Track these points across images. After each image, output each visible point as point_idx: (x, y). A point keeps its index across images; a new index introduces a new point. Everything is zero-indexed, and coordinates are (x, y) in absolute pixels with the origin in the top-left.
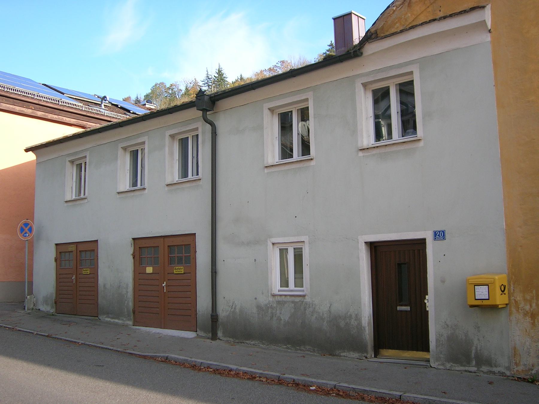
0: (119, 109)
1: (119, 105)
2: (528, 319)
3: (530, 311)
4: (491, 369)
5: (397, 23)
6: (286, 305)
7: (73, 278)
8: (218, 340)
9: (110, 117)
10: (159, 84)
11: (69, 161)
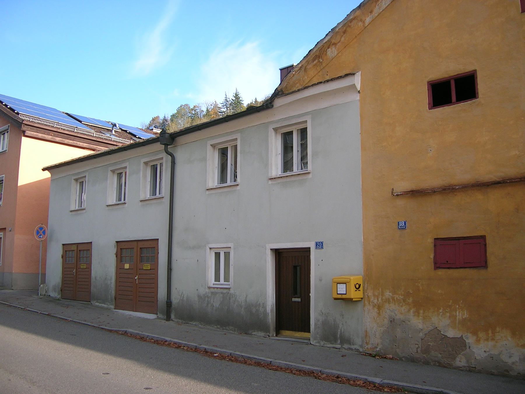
0: (128, 134)
1: (128, 131)
2: (376, 310)
3: (377, 304)
4: (350, 346)
5: (297, 84)
6: (217, 295)
7: (74, 271)
8: (171, 321)
9: (116, 142)
10: (184, 106)
11: (74, 179)
